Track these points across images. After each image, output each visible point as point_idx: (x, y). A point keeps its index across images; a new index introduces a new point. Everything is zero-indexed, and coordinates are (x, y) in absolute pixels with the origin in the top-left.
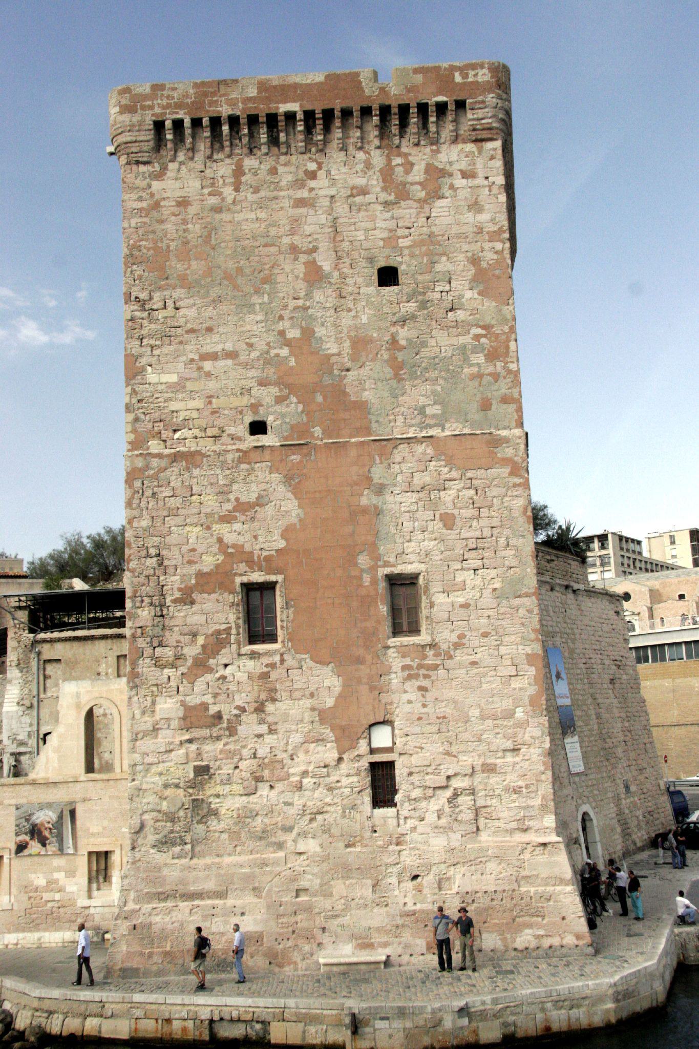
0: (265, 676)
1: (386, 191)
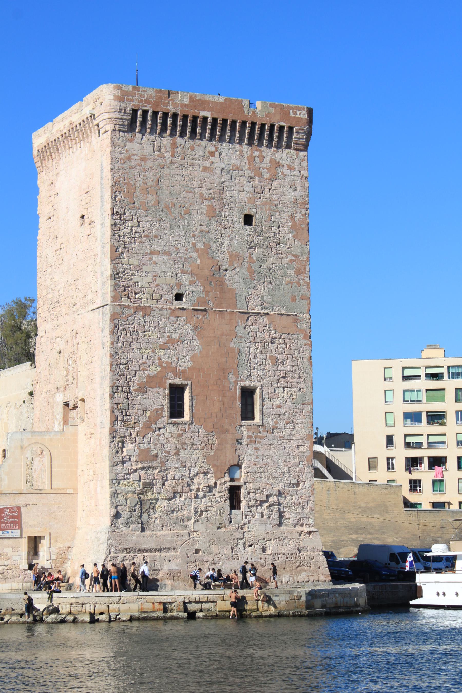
0: (180, 436)
1: (250, 170)
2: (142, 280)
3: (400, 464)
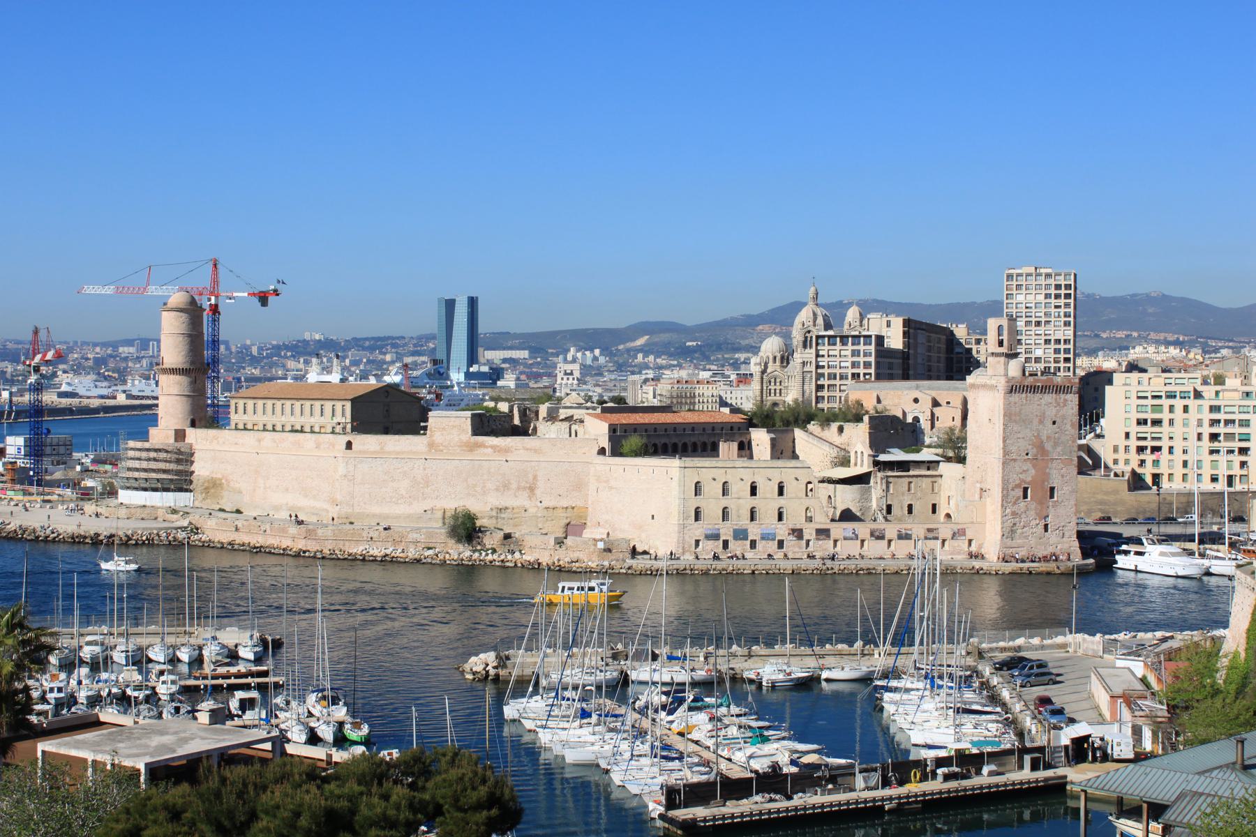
2: (1014, 449)
3: (1133, 449)
